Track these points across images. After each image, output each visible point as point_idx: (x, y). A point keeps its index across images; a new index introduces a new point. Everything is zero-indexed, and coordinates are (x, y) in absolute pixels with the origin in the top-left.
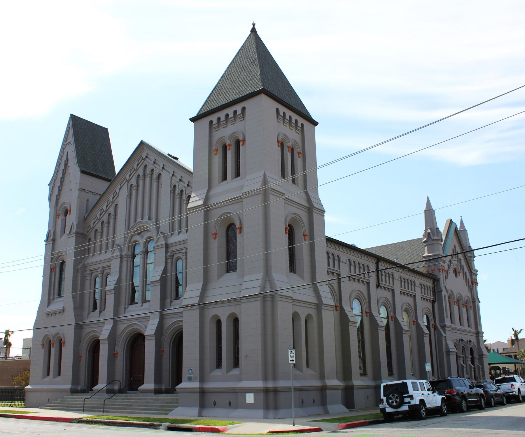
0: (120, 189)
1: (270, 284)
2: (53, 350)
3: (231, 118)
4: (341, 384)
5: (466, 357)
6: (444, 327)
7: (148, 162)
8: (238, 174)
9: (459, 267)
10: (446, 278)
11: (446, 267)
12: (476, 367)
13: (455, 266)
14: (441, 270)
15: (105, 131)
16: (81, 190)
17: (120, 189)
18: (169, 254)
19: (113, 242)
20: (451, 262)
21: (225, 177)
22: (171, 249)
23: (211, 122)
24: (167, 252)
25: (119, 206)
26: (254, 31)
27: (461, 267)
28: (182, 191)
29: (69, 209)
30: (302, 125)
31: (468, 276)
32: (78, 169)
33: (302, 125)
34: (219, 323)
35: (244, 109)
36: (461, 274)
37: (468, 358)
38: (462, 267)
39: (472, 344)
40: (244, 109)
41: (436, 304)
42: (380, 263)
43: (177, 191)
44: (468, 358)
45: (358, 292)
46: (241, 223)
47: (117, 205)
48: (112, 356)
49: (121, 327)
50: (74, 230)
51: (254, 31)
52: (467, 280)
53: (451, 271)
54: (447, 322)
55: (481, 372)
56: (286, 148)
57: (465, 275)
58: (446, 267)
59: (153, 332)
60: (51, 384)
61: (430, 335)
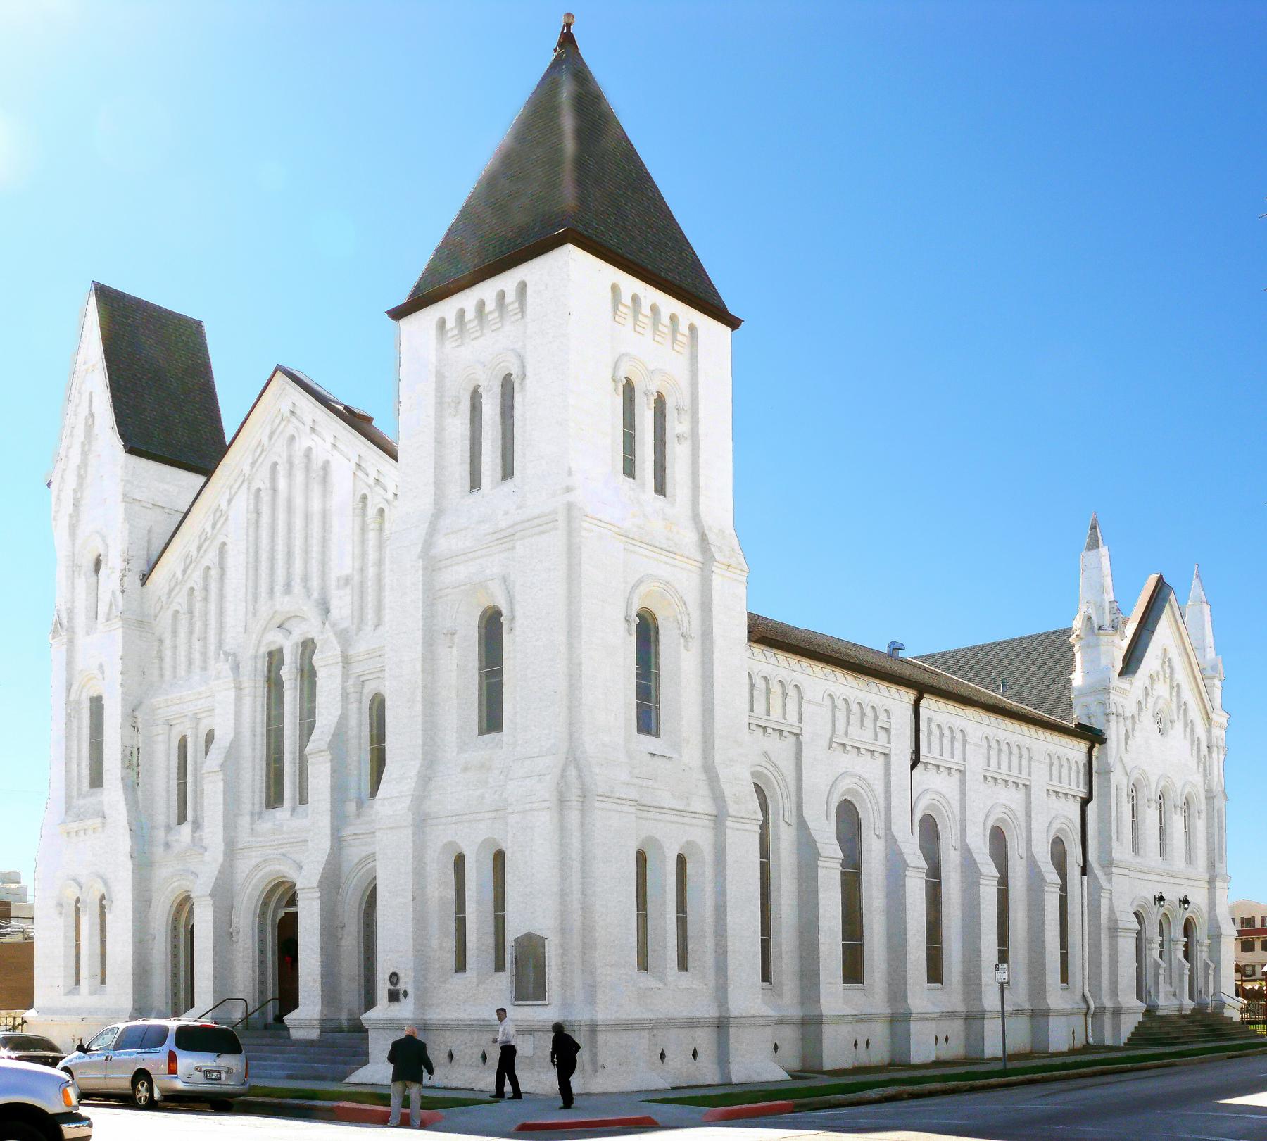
0: (230, 501)
1: (578, 769)
2: (84, 920)
3: (491, 312)
4: (772, 1013)
5: (1171, 940)
6: (1108, 864)
7: (297, 428)
8: (507, 472)
9: (1174, 707)
10: (1127, 737)
11: (1131, 709)
12: (1200, 965)
13: (1161, 704)
14: (1113, 718)
15: (199, 324)
16: (129, 500)
17: (230, 501)
18: (351, 682)
19: (220, 644)
20: (1147, 695)
21: (475, 482)
22: (356, 669)
23: (442, 323)
24: (346, 676)
25: (229, 547)
26: (567, 40)
27: (1179, 708)
28: (382, 511)
29: (515, 370)
30: (692, 328)
31: (1200, 731)
32: (119, 444)
33: (692, 328)
34: (460, 861)
35: (522, 287)
36: (1179, 726)
37: (1176, 942)
38: (1183, 707)
39: (1191, 907)
40: (522, 287)
41: (1092, 807)
42: (923, 703)
43: (372, 512)
44: (1176, 942)
45: (855, 780)
46: (512, 611)
47: (224, 544)
48: (224, 935)
49: (244, 866)
50: (116, 613)
51: (567, 40)
52: (1195, 742)
53: (1147, 720)
54: (1121, 851)
55: (1211, 978)
56: (640, 399)
57: (1189, 725)
58: (1131, 709)
59: (315, 881)
60: (1100, 832)
61: (1063, 889)
